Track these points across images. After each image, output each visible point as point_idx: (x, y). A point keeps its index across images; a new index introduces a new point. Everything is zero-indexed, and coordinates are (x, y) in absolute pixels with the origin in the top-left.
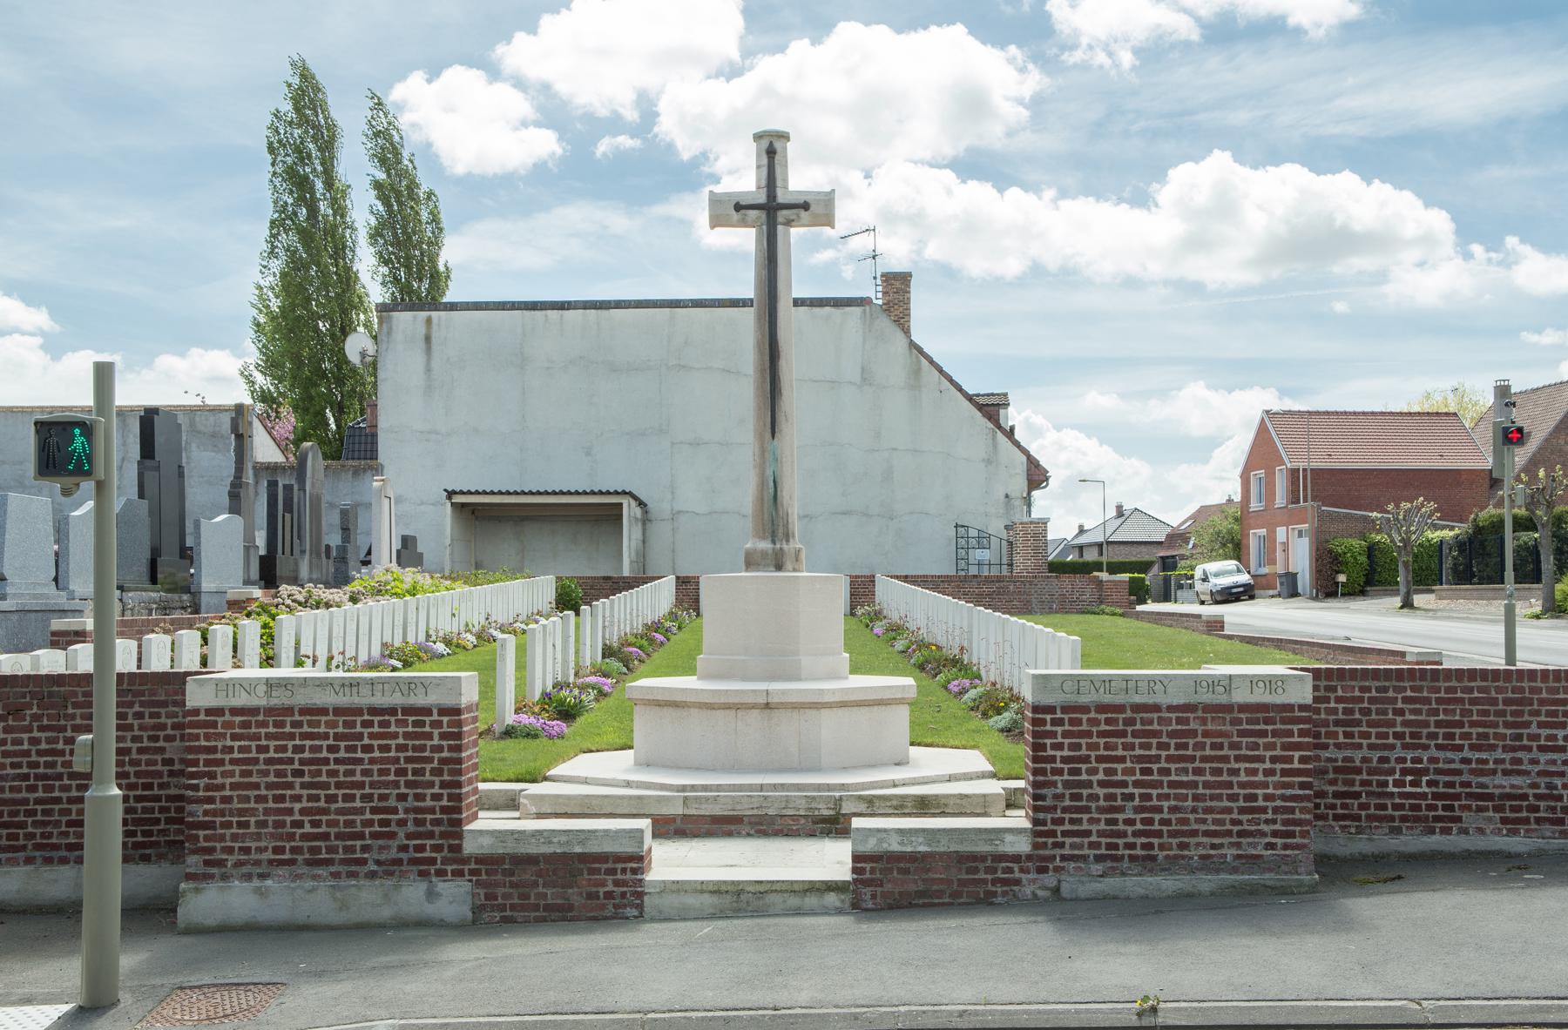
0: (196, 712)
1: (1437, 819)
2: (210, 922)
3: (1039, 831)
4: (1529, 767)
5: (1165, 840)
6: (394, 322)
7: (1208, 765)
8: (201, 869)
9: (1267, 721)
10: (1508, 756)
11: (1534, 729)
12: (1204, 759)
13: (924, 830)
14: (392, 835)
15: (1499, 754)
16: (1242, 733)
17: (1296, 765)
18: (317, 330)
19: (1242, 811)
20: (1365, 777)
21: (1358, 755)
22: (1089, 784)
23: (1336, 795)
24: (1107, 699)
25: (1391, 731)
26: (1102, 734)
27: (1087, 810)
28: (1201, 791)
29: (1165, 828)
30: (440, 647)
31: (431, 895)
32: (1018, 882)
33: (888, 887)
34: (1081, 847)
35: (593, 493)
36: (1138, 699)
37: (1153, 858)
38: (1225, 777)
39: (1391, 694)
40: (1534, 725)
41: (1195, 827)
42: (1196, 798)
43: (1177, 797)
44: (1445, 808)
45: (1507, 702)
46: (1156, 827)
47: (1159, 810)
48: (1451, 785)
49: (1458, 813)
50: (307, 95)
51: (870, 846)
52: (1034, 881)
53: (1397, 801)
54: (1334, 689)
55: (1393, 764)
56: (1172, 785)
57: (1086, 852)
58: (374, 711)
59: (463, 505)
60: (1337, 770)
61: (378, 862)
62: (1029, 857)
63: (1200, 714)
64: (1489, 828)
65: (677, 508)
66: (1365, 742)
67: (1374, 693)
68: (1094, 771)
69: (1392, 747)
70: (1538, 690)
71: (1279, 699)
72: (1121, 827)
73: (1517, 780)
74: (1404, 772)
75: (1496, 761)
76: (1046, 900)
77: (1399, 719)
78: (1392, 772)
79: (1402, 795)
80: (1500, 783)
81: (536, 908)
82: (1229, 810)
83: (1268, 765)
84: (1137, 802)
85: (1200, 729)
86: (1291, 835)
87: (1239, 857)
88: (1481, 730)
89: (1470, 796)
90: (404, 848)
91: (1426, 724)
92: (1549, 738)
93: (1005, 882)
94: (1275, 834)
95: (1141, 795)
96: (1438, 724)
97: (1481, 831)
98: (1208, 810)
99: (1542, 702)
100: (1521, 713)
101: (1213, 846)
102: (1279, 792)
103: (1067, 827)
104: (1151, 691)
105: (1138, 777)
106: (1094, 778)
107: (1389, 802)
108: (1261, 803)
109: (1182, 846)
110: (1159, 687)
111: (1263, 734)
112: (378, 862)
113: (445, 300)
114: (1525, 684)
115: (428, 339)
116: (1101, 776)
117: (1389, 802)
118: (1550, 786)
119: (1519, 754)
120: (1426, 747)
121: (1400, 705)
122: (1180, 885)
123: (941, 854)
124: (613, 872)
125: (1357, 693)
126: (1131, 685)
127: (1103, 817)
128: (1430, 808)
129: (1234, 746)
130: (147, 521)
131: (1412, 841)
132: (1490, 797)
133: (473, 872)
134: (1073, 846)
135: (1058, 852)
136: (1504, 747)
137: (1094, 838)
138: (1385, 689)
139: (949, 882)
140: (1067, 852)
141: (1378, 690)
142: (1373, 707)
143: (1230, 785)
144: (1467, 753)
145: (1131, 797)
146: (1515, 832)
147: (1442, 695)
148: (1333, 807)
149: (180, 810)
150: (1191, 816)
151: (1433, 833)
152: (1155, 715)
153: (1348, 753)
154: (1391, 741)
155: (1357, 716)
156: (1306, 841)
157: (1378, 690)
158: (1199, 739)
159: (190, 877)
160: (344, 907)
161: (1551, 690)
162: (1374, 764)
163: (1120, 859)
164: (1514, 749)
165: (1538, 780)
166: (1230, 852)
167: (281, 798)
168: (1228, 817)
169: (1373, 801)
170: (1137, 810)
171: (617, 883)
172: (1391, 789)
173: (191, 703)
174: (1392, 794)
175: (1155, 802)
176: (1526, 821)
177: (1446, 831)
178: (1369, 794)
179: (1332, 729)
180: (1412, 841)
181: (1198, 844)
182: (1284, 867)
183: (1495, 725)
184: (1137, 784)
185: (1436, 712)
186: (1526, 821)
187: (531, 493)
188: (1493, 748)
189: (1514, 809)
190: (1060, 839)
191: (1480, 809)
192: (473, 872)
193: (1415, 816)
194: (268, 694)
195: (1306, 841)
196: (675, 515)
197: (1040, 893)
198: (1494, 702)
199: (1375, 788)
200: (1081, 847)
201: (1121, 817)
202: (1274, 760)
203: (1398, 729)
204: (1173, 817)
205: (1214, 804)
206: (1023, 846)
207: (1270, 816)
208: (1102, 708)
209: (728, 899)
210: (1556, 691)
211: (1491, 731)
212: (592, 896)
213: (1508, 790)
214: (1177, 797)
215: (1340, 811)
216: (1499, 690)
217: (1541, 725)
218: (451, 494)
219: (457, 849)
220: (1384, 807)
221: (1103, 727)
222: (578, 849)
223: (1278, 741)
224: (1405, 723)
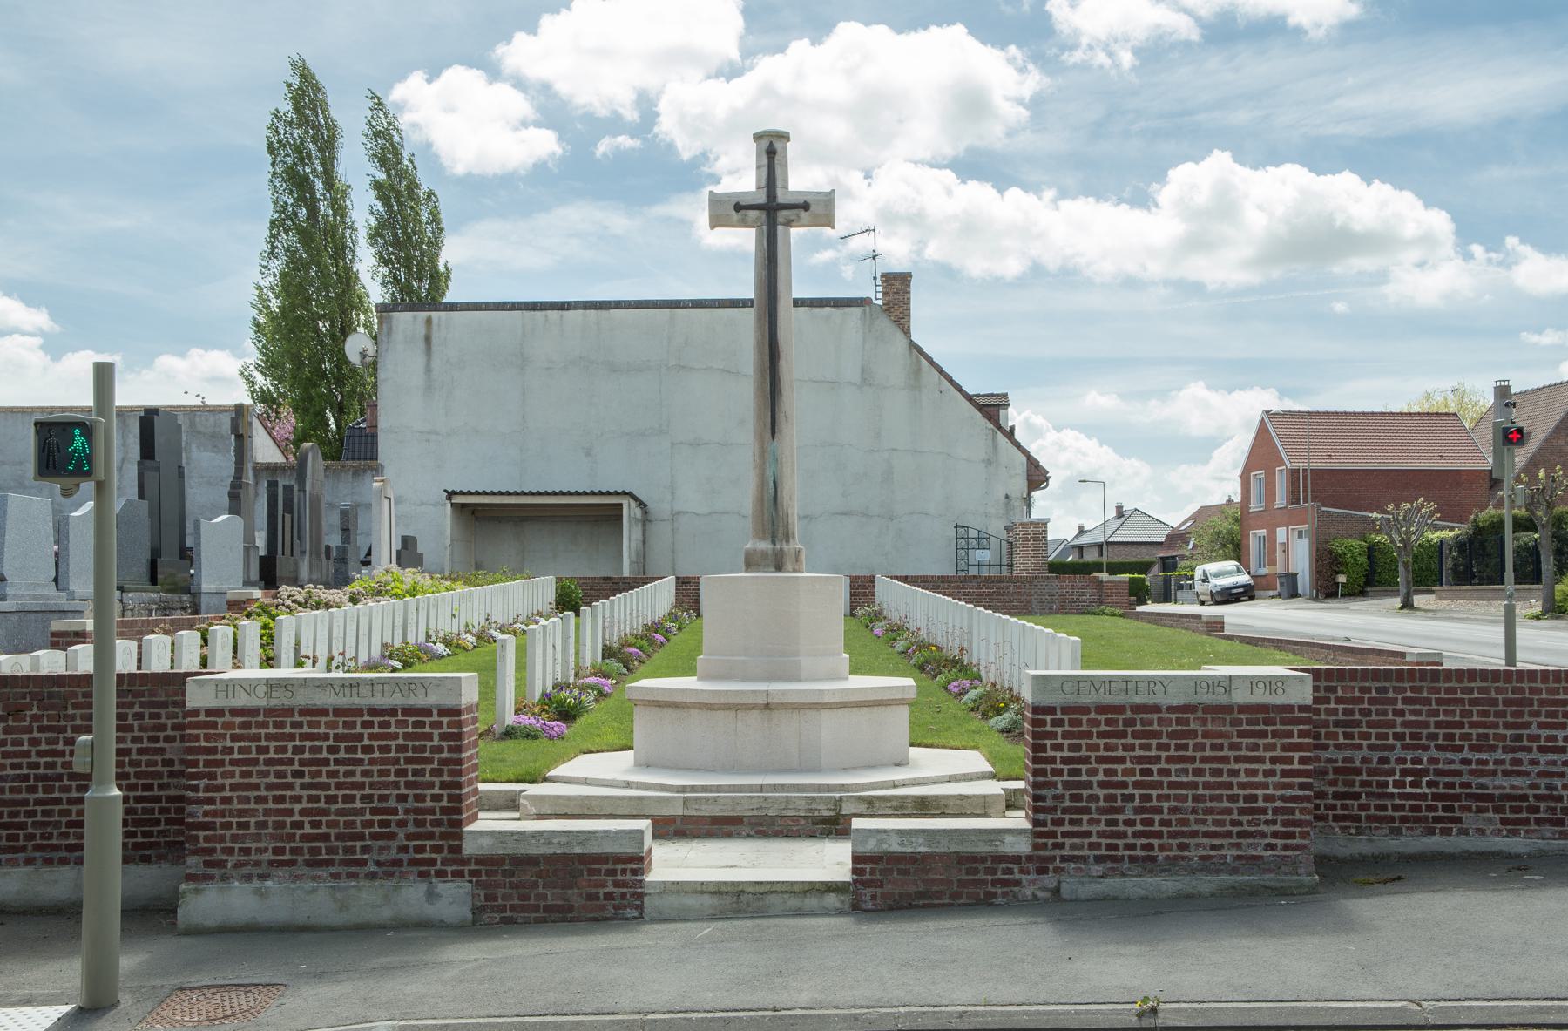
0: (196, 712)
1: (1437, 820)
2: (210, 922)
3: (1039, 832)
4: (1530, 768)
5: (1165, 840)
7: (1207, 766)
8: (201, 870)
10: (1507, 757)
11: (1534, 730)
12: (1204, 760)
13: (924, 831)
14: (392, 836)
15: (1499, 755)
16: (1242, 734)
17: (1296, 766)
18: (317, 330)
19: (1242, 811)
20: (1365, 777)
21: (1358, 756)
22: (1089, 785)
23: (1336, 796)
24: (1107, 700)
25: (1391, 731)
26: (1102, 735)
27: (1087, 811)
28: (1201, 792)
29: (1165, 829)
30: (440, 648)
31: (431, 896)
32: (1018, 883)
33: (888, 888)
35: (593, 493)
36: (1138, 700)
37: (1153, 859)
38: (1225, 778)
39: (1391, 695)
40: (1534, 725)
41: (1195, 828)
42: (1196, 799)
43: (1177, 798)
44: (1445, 809)
45: (1507, 702)
46: (1156, 828)
47: (1159, 811)
48: (1451, 785)
49: (1458, 814)
50: (307, 95)
51: (870, 847)
52: (1034, 882)
53: (1397, 801)
55: (1393, 765)
56: (1172, 785)
57: (1086, 852)
58: (374, 711)
59: (463, 506)
60: (1337, 771)
61: (378, 863)
62: (1029, 858)
63: (1200, 714)
64: (1489, 829)
65: (677, 508)
66: (1365, 743)
67: (1374, 694)
68: (1093, 772)
69: (1392, 748)
70: (1539, 691)
71: (1279, 700)
72: (1121, 828)
73: (1517, 781)
74: (1404, 773)
75: (1497, 762)
76: (1046, 901)
77: (1399, 720)
78: (1392, 772)
79: (1401, 796)
80: (1500, 784)
81: (536, 908)
82: (1229, 811)
83: (1268, 766)
84: (1137, 803)
85: (1200, 729)
86: (1291, 835)
87: (1239, 857)
88: (1480, 731)
89: (1469, 796)
90: (404, 849)
91: (1426, 725)
92: (1549, 739)
93: (1005, 883)
94: (1275, 835)
95: (1141, 796)
96: (1438, 725)
97: (1481, 832)
98: (1207, 811)
99: (1542, 703)
100: (1521, 714)
101: (1213, 847)
102: (1279, 793)
103: (1067, 828)
104: (1151, 692)
105: (1138, 777)
106: (1094, 779)
108: (1261, 804)
109: (1182, 847)
110: (1159, 688)
111: (1263, 734)
112: (378, 863)
113: (445, 300)
115: (428, 339)
116: (1101, 777)
118: (1550, 787)
119: (1519, 755)
120: (1426, 748)
121: (1400, 706)
122: (1181, 886)
123: (941, 855)
124: (613, 872)
125: (1357, 694)
126: (1131, 685)
127: (1103, 817)
128: (1430, 808)
129: (1233, 747)
130: (147, 522)
131: (1412, 842)
132: (1490, 798)
133: (473, 873)
134: (1073, 847)
135: (1058, 853)
136: (1504, 748)
137: (1094, 839)
138: (1385, 690)
139: (949, 882)
140: (1067, 852)
141: (1378, 690)
142: (1373, 708)
143: (1229, 786)
144: (1467, 754)
145: (1131, 798)
146: (1515, 833)
147: (1442, 695)
148: (1333, 807)
149: (180, 810)
150: (1191, 817)
151: (1433, 833)
152: (1155, 716)
153: (1348, 754)
154: (1391, 741)
155: (1357, 717)
157: (1378, 690)
158: (1199, 740)
159: (190, 878)
161: (1550, 691)
162: (1374, 764)
163: (1120, 860)
164: (1513, 750)
165: (1538, 781)
166: (1230, 853)
169: (1373, 802)
170: (1138, 811)
174: (1392, 795)
175: (1155, 803)
176: (1526, 822)
177: (1446, 832)
179: (1332, 729)
180: (1412, 842)
181: (1198, 845)
182: (1284, 868)
184: (1137, 785)
185: (1435, 713)
186: (1526, 822)
187: (531, 493)
188: (1493, 748)
189: (1514, 810)
190: (1060, 840)
191: (1480, 810)
192: (473, 873)
193: (1415, 817)
194: (268, 694)
197: (1040, 894)
198: (1494, 702)
199: (1374, 789)
201: (1121, 817)
202: (1274, 760)
203: (1399, 730)
204: (1173, 818)
205: (1213, 804)
206: (1023, 847)
207: (1269, 817)
208: (1102, 709)
209: (728, 900)
211: (1491, 731)
212: (592, 897)
213: (1508, 791)
214: (1177, 798)
215: (1339, 812)
216: (1499, 691)
217: (1541, 726)
218: (451, 495)
220: (1384, 808)
221: (1104, 728)
222: (578, 850)
223: (1279, 742)
224: (1406, 724)
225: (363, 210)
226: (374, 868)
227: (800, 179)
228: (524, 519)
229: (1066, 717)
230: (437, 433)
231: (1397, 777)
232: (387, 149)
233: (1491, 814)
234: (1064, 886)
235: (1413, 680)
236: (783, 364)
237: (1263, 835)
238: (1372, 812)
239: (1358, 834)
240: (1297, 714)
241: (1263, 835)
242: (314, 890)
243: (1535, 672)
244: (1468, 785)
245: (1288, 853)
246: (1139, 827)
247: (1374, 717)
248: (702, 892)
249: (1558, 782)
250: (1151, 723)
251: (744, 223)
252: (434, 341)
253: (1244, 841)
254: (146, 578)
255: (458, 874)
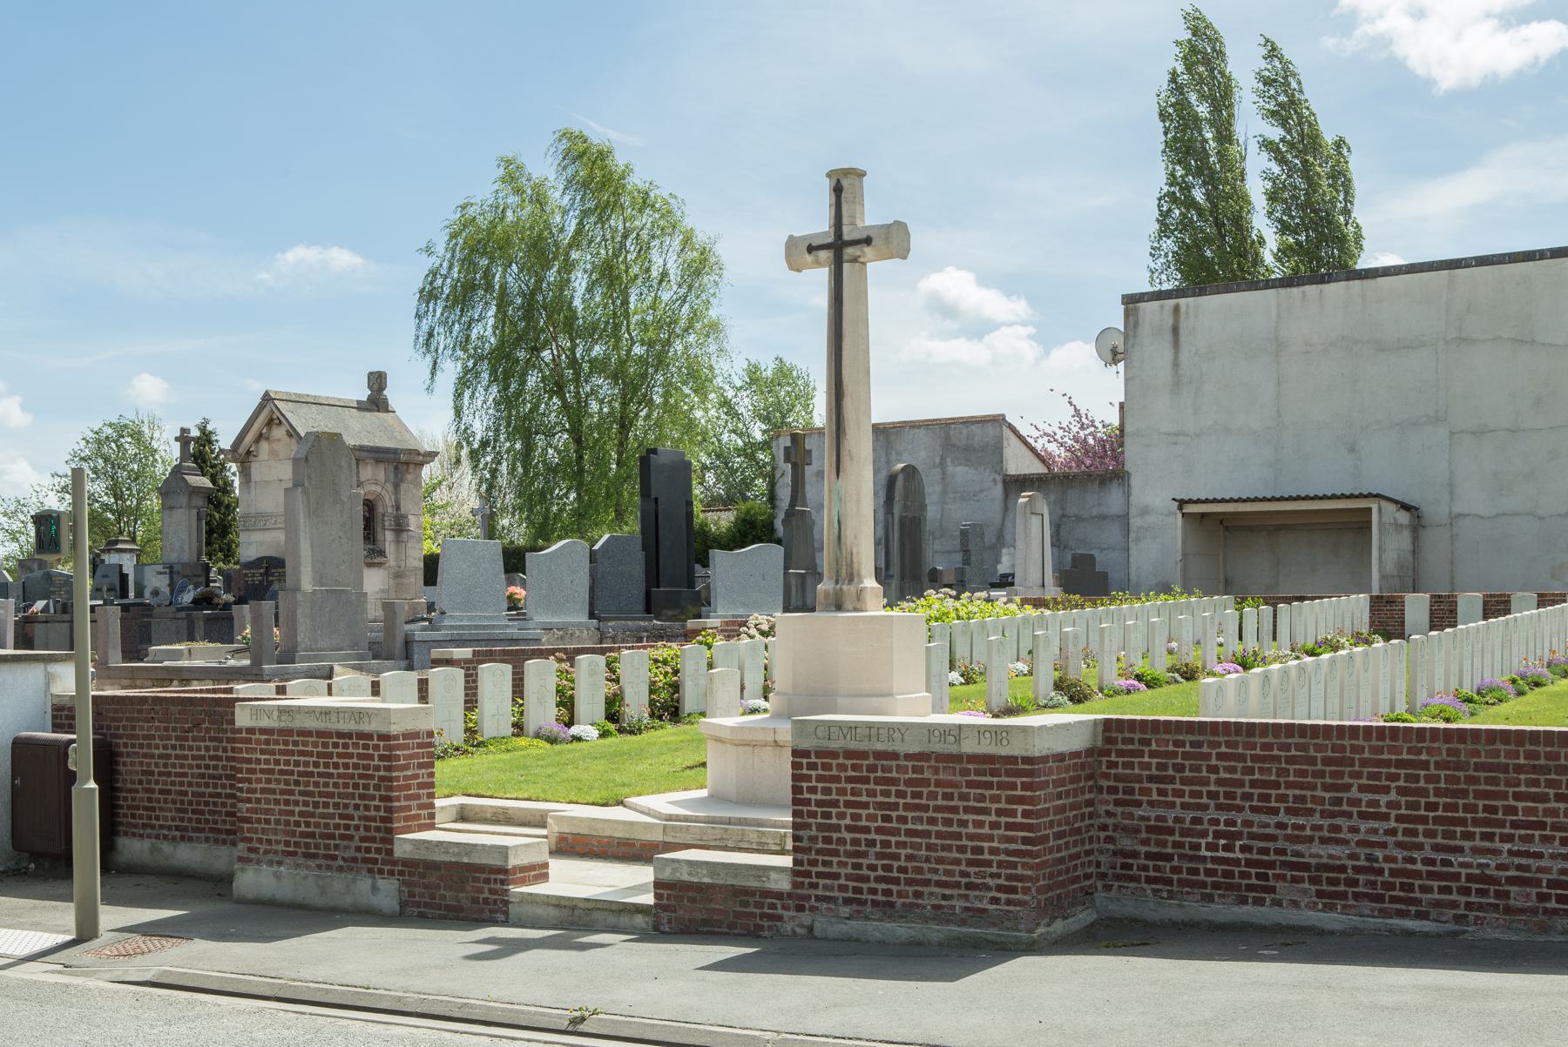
0: (240, 731)
1: (1250, 888)
2: (250, 896)
3: (797, 872)
4: (1349, 836)
6: (1141, 313)
7: (940, 815)
8: (245, 854)
9: (993, 773)
10: (1326, 823)
11: (1354, 793)
12: (937, 809)
13: (707, 863)
14: (351, 838)
15: (1317, 820)
16: (970, 784)
17: (1019, 819)
19: (970, 863)
20: (1177, 838)
22: (837, 828)
23: (1149, 856)
24: (853, 745)
26: (850, 780)
27: (835, 853)
28: (933, 841)
31: (375, 889)
32: (780, 918)
33: (680, 913)
34: (831, 888)
36: (880, 747)
37: (892, 905)
38: (955, 829)
39: (1205, 749)
40: (1355, 789)
41: (928, 876)
42: (929, 847)
43: (913, 846)
44: (1258, 876)
45: (1326, 761)
47: (896, 857)
48: (1265, 851)
49: (1271, 883)
50: (1202, 52)
51: (667, 875)
52: (793, 918)
53: (1210, 866)
54: (1147, 742)
55: (1206, 826)
56: (909, 833)
57: (836, 894)
58: (340, 735)
60: (1150, 829)
61: (344, 859)
62: (790, 895)
63: (933, 763)
65: (1457, 509)
66: (1178, 800)
67: (1188, 749)
68: (841, 816)
69: (1205, 807)
71: (1004, 751)
72: (865, 872)
73: (1334, 850)
74: (1218, 835)
75: (1314, 828)
77: (1213, 777)
78: (1204, 834)
79: (1215, 860)
80: (1319, 852)
81: (439, 907)
82: (957, 862)
83: (993, 818)
84: (878, 849)
85: (933, 778)
86: (1013, 890)
87: (967, 909)
88: (1298, 792)
89: (1284, 864)
90: (358, 849)
91: (1241, 783)
92: (1371, 803)
93: (771, 917)
94: (999, 888)
95: (882, 842)
96: (1253, 784)
97: (1295, 904)
98: (940, 861)
99: (1364, 763)
100: (1340, 775)
101: (945, 897)
102: (1002, 846)
103: (820, 869)
104: (891, 739)
105: (880, 823)
106: (843, 823)
107: (1201, 867)
108: (986, 856)
109: (918, 895)
110: (897, 735)
111: (989, 785)
112: (344, 859)
114: (1346, 742)
115: (1175, 330)
116: (848, 821)
117: (1201, 867)
118: (1370, 858)
119: (1339, 821)
120: (1240, 809)
121: (1214, 762)
122: (912, 932)
123: (721, 887)
124: (487, 881)
125: (1171, 748)
126: (874, 732)
127: (850, 861)
128: (1244, 875)
129: (964, 797)
130: (641, 555)
131: (1223, 910)
132: (1305, 867)
133: (401, 873)
134: (826, 888)
135: (813, 892)
137: (842, 881)
138: (1199, 744)
140: (820, 892)
141: (1193, 744)
142: (1187, 763)
143: (958, 836)
144: (1282, 817)
145: (872, 843)
146: (1330, 908)
147: (1258, 752)
148: (1145, 868)
149: (233, 805)
150: (925, 865)
151: (1246, 903)
152: (894, 763)
153: (1161, 812)
154: (1205, 800)
155: (1171, 772)
156: (1027, 898)
157: (1193, 744)
158: (932, 788)
159: (240, 859)
160: (323, 893)
161: (1374, 750)
162: (1187, 825)
163: (862, 903)
164: (1332, 815)
165: (1358, 850)
166: (959, 904)
167: (287, 802)
168: (957, 868)
169: (1185, 865)
170: (880, 856)
171: (492, 891)
172: (1204, 853)
173: (239, 724)
174: (1205, 858)
175: (893, 850)
176: (1344, 896)
177: (1259, 902)
178: (1181, 857)
179: (1145, 785)
180: (1223, 910)
181: (931, 894)
183: (1313, 787)
184: (879, 830)
185: (1251, 771)
186: (1344, 896)
188: (1310, 812)
189: (1331, 882)
190: (814, 880)
191: (1295, 880)
192: (401, 873)
193: (1227, 884)
194: (279, 717)
195: (1027, 898)
196: (1454, 518)
197: (798, 930)
198: (1311, 761)
199: (1187, 851)
200: (831, 888)
201: (865, 862)
202: (999, 812)
203: (1212, 788)
204: (910, 865)
205: (944, 854)
206: (784, 884)
207: (994, 870)
208: (850, 754)
209: (566, 912)
210: (1380, 750)
211: (1308, 793)
212: (475, 901)
213: (1325, 860)
214: (913, 846)
215: (1152, 874)
216: (1318, 748)
217: (1362, 789)
218: (1182, 503)
219: (390, 852)
221: (851, 773)
222: (465, 860)
223: (1004, 793)
224: (1219, 782)
225: (1258, 176)
226: (341, 863)
227: (871, 214)
228: (1279, 528)
229: (819, 761)
230: (1185, 435)
231: (1210, 839)
232: (1286, 106)
233: (1306, 885)
234: (817, 924)
235: (1192, 733)
236: (848, 403)
237: (988, 888)
238: (1184, 875)
239: (1170, 898)
240: (1021, 766)
241: (988, 888)
242: (306, 877)
243: (1134, 721)
244: (1282, 852)
245: (1011, 908)
246: (880, 872)
247: (1187, 773)
248: (548, 905)
249: (1379, 854)
250: (890, 771)
251: (818, 264)
252: (1182, 332)
253: (971, 893)
254: (641, 607)
255: (391, 873)
